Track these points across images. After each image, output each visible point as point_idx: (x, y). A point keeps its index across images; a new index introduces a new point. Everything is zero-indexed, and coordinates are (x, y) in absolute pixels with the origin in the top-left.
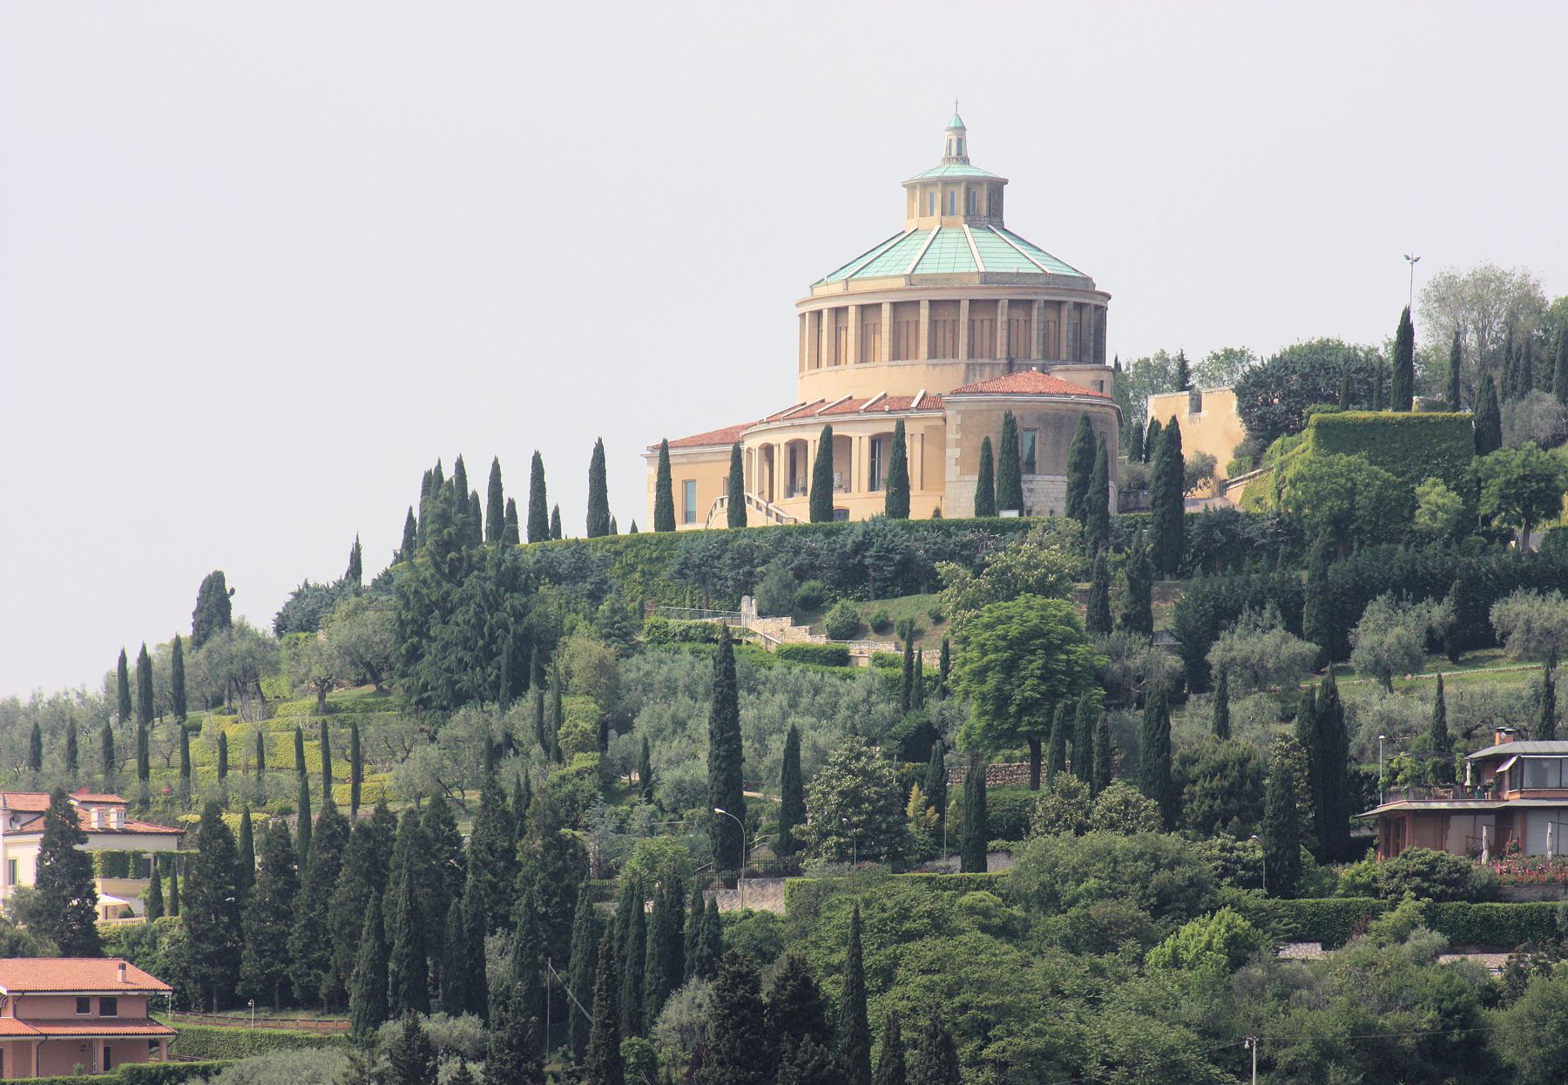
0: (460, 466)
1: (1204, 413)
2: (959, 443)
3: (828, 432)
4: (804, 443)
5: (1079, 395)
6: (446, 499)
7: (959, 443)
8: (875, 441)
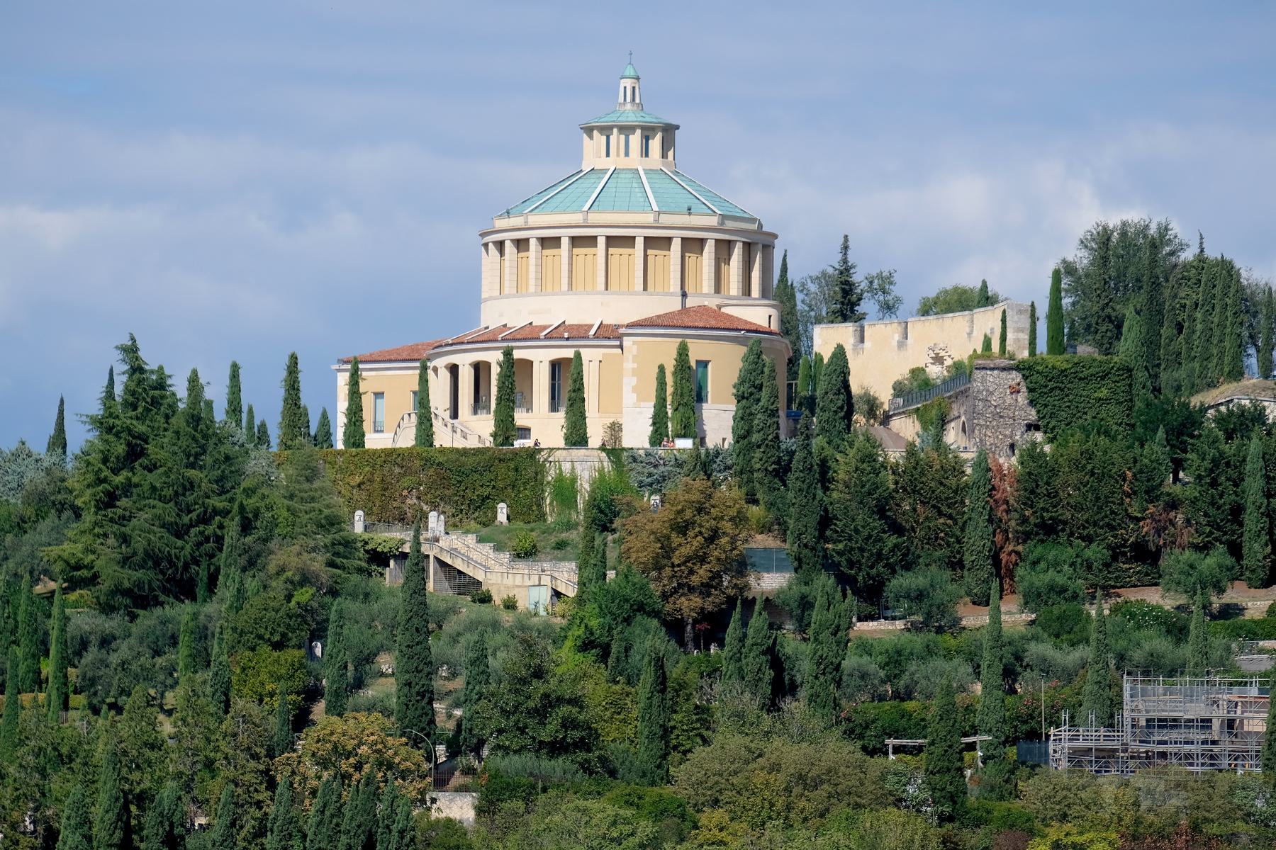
0: (194, 381)
1: (867, 344)
2: (634, 372)
3: (508, 353)
4: (488, 365)
5: (748, 331)
6: (144, 392)
7: (634, 372)
8: (555, 366)
